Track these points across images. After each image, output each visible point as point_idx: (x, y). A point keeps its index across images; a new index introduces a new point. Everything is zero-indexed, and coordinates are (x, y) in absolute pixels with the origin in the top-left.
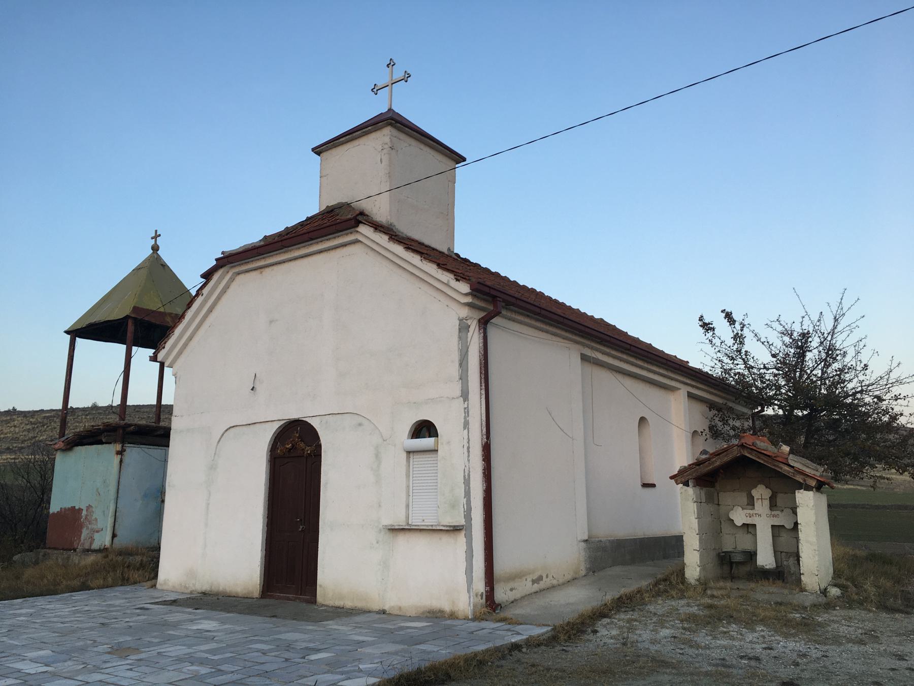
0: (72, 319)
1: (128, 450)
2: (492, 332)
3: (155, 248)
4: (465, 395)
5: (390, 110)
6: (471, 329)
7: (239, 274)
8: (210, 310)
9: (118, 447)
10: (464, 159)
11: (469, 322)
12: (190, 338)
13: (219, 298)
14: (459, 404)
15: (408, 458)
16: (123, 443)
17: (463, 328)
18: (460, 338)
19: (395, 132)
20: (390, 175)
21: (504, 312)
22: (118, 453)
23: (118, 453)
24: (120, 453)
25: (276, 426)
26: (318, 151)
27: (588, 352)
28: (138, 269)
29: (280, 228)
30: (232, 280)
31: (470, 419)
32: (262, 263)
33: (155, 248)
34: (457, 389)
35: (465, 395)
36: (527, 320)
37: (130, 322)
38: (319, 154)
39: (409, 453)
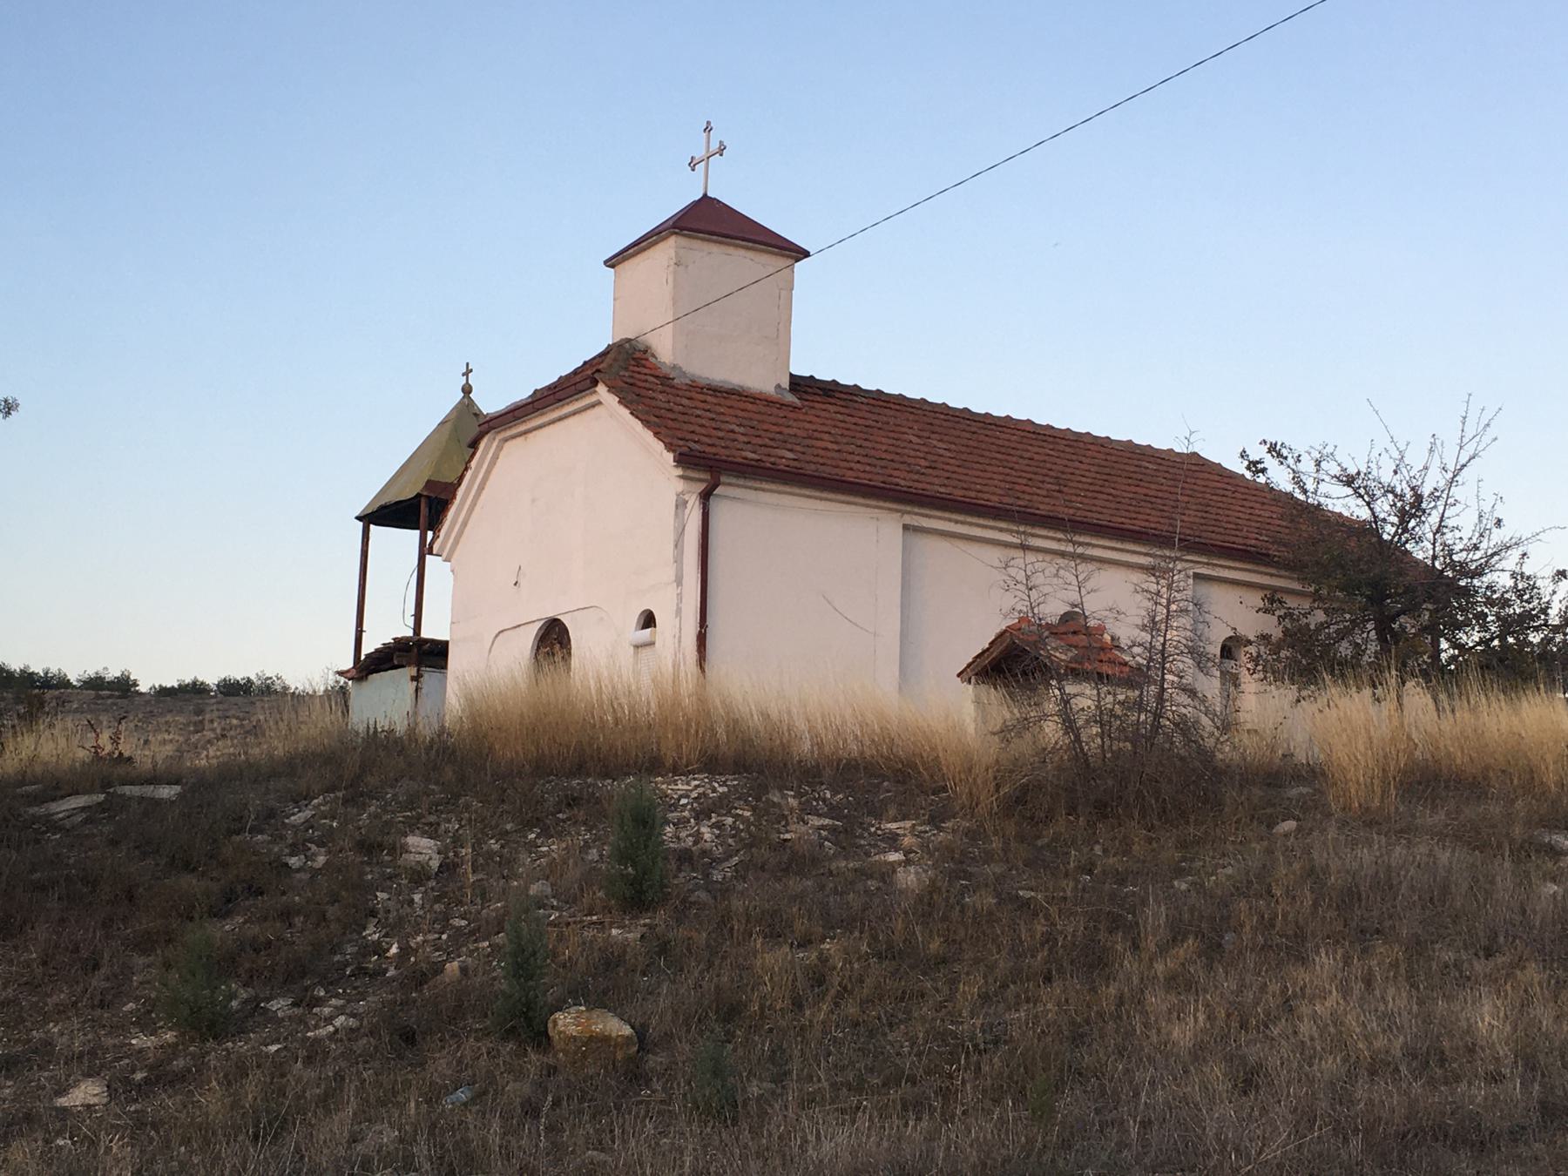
0: (362, 503)
1: (426, 676)
2: (720, 509)
3: (467, 390)
4: (679, 581)
5: (705, 195)
6: (689, 505)
7: (506, 440)
8: (481, 488)
9: (413, 671)
10: (806, 254)
11: (686, 497)
12: (465, 524)
13: (488, 472)
14: (672, 591)
15: (636, 654)
16: (419, 665)
17: (681, 504)
18: (676, 514)
19: (682, 241)
20: (675, 301)
21: (723, 479)
22: (413, 679)
23: (413, 679)
24: (415, 679)
25: (539, 625)
26: (612, 262)
27: (908, 519)
28: (443, 423)
29: (552, 379)
30: (500, 448)
31: (683, 606)
32: (522, 428)
33: (467, 390)
34: (671, 573)
35: (679, 581)
36: (773, 487)
37: (423, 500)
38: (612, 266)
39: (637, 647)
